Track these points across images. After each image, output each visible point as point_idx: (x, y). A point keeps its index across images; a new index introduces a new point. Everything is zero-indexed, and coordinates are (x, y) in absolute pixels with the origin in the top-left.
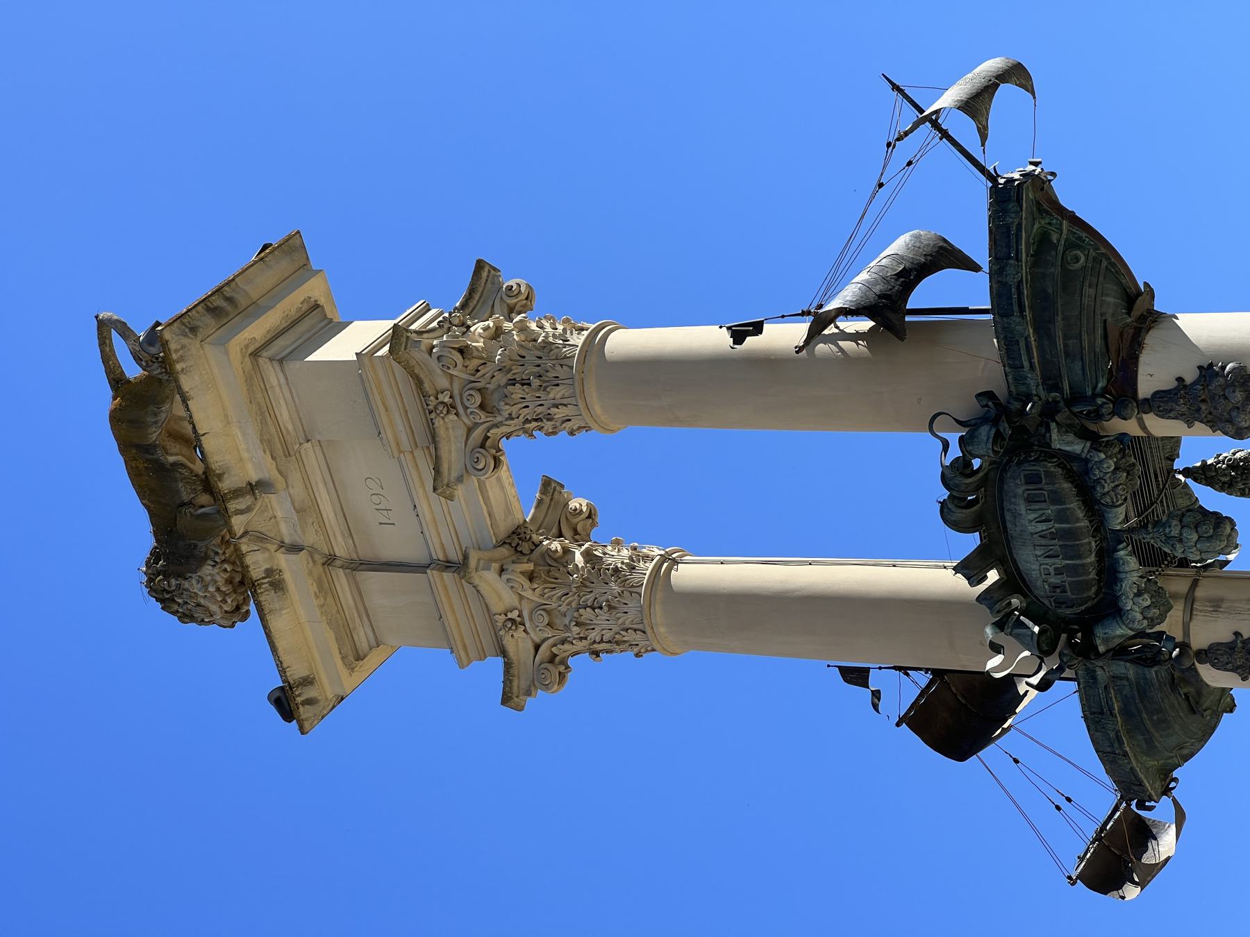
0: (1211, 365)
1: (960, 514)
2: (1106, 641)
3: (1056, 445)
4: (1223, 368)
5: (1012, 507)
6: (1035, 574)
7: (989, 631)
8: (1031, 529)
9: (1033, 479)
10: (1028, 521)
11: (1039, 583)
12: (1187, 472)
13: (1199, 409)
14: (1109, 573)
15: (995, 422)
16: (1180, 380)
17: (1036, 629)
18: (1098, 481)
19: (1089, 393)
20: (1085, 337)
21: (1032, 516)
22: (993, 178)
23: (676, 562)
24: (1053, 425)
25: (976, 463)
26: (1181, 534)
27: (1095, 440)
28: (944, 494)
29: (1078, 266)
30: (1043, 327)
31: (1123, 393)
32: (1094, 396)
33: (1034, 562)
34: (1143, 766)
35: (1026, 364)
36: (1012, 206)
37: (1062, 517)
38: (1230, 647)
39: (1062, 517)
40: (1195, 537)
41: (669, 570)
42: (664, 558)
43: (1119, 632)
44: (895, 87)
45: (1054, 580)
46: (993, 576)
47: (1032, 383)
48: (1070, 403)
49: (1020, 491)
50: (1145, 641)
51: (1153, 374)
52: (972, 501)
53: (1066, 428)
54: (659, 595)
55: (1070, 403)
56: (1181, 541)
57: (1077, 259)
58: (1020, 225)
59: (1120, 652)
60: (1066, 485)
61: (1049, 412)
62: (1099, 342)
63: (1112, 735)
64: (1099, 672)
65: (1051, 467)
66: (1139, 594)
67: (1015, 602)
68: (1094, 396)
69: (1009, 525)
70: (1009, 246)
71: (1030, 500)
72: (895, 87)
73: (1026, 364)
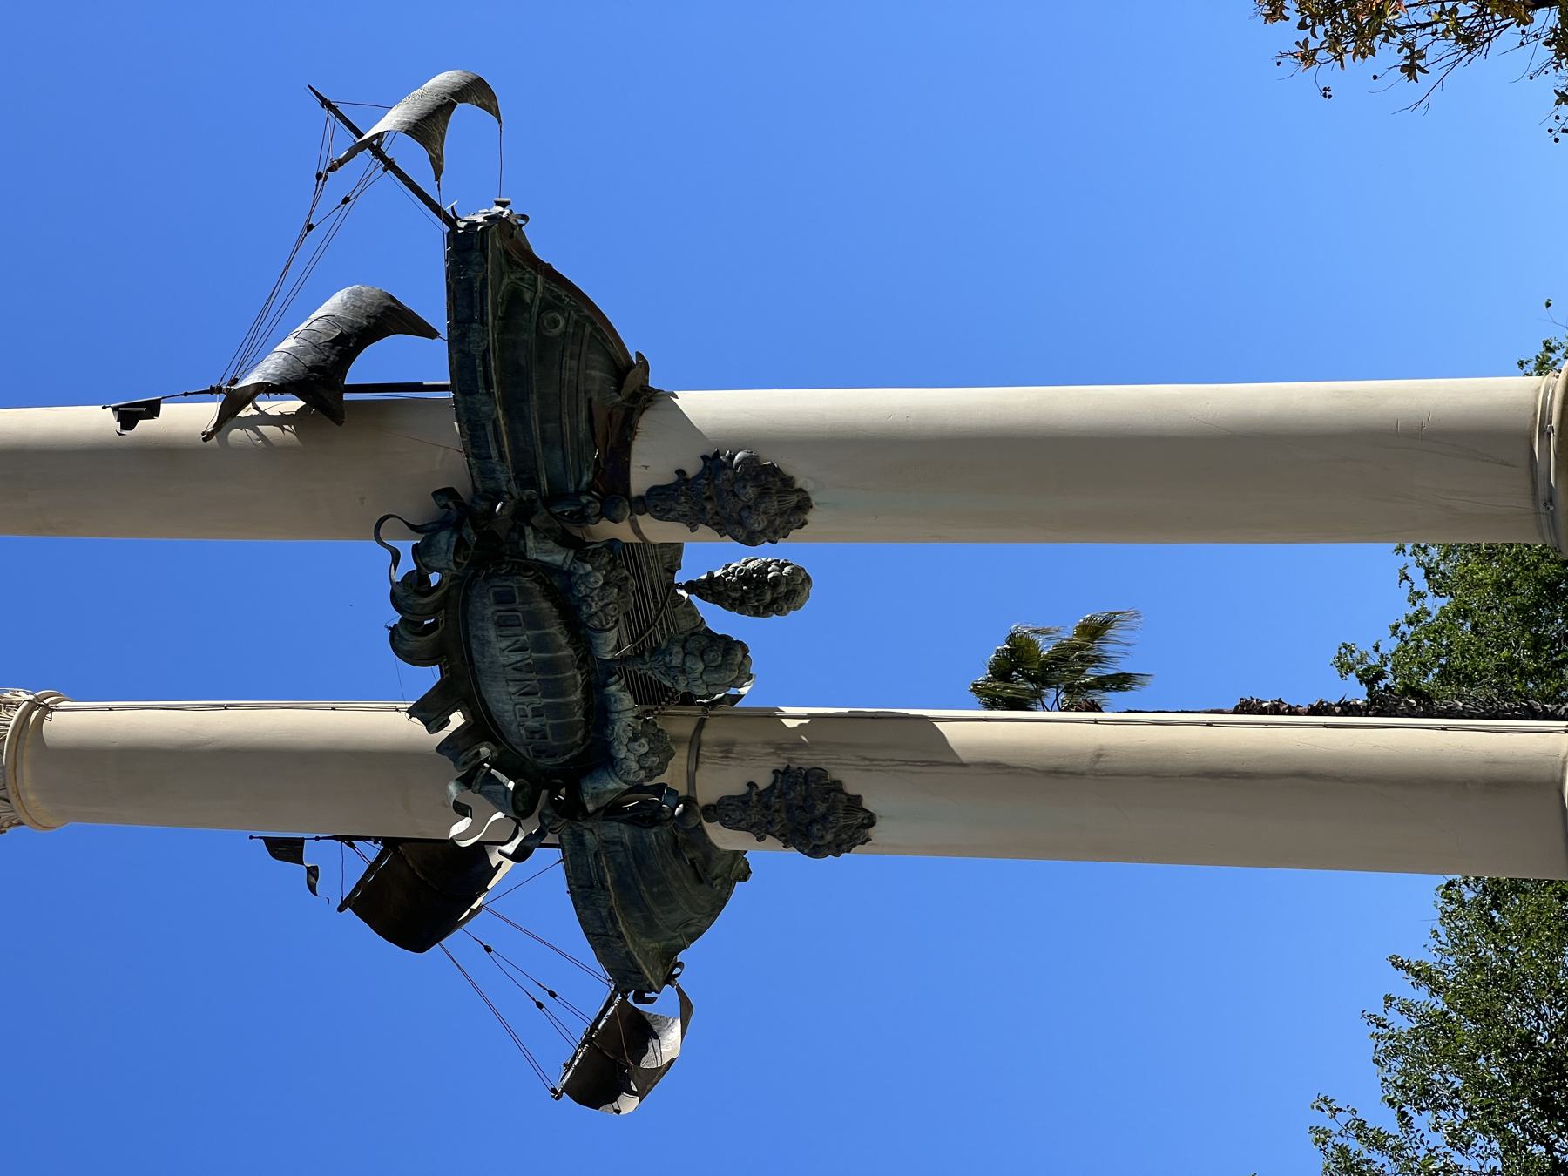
0: (717, 455)
1: (414, 643)
2: (595, 797)
3: (533, 555)
4: (732, 458)
5: (479, 633)
6: (508, 716)
7: (453, 789)
8: (502, 660)
9: (504, 598)
10: (499, 650)
11: (514, 727)
12: (691, 587)
13: (703, 509)
14: (599, 713)
15: (457, 526)
16: (680, 472)
17: (511, 785)
18: (583, 599)
19: (572, 489)
20: (566, 419)
21: (504, 644)
22: (451, 221)
23: (49, 709)
24: (528, 530)
25: (434, 578)
26: (684, 663)
27: (580, 548)
28: (395, 617)
29: (556, 331)
30: (514, 409)
31: (613, 491)
32: (578, 493)
33: (505, 700)
34: (641, 949)
35: (494, 453)
36: (475, 256)
37: (541, 644)
38: (744, 801)
39: (541, 644)
40: (700, 666)
41: (40, 720)
42: (33, 705)
43: (611, 786)
44: (326, 103)
45: (532, 723)
46: (457, 719)
47: (502, 477)
48: (548, 502)
49: (489, 612)
50: (643, 796)
51: (649, 465)
52: (431, 627)
53: (543, 534)
54: (27, 753)
55: (548, 502)
56: (683, 672)
57: (555, 323)
58: (485, 279)
59: (613, 811)
60: (545, 605)
61: (523, 513)
62: (583, 426)
63: (604, 912)
64: (588, 836)
65: (526, 582)
66: (634, 739)
67: (485, 751)
68: (578, 493)
69: (476, 656)
70: (471, 306)
71: (501, 624)
72: (326, 103)
73: (494, 453)
